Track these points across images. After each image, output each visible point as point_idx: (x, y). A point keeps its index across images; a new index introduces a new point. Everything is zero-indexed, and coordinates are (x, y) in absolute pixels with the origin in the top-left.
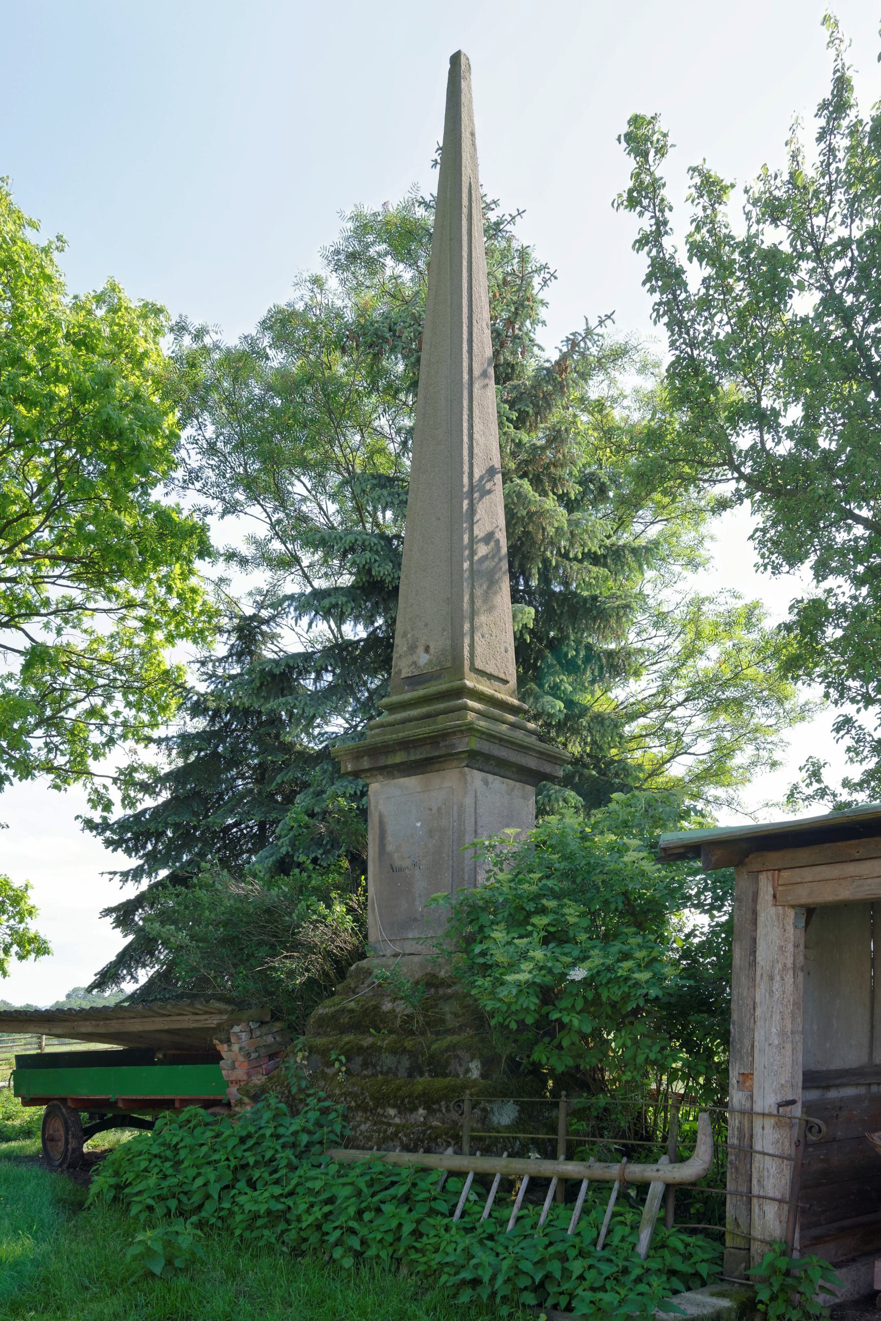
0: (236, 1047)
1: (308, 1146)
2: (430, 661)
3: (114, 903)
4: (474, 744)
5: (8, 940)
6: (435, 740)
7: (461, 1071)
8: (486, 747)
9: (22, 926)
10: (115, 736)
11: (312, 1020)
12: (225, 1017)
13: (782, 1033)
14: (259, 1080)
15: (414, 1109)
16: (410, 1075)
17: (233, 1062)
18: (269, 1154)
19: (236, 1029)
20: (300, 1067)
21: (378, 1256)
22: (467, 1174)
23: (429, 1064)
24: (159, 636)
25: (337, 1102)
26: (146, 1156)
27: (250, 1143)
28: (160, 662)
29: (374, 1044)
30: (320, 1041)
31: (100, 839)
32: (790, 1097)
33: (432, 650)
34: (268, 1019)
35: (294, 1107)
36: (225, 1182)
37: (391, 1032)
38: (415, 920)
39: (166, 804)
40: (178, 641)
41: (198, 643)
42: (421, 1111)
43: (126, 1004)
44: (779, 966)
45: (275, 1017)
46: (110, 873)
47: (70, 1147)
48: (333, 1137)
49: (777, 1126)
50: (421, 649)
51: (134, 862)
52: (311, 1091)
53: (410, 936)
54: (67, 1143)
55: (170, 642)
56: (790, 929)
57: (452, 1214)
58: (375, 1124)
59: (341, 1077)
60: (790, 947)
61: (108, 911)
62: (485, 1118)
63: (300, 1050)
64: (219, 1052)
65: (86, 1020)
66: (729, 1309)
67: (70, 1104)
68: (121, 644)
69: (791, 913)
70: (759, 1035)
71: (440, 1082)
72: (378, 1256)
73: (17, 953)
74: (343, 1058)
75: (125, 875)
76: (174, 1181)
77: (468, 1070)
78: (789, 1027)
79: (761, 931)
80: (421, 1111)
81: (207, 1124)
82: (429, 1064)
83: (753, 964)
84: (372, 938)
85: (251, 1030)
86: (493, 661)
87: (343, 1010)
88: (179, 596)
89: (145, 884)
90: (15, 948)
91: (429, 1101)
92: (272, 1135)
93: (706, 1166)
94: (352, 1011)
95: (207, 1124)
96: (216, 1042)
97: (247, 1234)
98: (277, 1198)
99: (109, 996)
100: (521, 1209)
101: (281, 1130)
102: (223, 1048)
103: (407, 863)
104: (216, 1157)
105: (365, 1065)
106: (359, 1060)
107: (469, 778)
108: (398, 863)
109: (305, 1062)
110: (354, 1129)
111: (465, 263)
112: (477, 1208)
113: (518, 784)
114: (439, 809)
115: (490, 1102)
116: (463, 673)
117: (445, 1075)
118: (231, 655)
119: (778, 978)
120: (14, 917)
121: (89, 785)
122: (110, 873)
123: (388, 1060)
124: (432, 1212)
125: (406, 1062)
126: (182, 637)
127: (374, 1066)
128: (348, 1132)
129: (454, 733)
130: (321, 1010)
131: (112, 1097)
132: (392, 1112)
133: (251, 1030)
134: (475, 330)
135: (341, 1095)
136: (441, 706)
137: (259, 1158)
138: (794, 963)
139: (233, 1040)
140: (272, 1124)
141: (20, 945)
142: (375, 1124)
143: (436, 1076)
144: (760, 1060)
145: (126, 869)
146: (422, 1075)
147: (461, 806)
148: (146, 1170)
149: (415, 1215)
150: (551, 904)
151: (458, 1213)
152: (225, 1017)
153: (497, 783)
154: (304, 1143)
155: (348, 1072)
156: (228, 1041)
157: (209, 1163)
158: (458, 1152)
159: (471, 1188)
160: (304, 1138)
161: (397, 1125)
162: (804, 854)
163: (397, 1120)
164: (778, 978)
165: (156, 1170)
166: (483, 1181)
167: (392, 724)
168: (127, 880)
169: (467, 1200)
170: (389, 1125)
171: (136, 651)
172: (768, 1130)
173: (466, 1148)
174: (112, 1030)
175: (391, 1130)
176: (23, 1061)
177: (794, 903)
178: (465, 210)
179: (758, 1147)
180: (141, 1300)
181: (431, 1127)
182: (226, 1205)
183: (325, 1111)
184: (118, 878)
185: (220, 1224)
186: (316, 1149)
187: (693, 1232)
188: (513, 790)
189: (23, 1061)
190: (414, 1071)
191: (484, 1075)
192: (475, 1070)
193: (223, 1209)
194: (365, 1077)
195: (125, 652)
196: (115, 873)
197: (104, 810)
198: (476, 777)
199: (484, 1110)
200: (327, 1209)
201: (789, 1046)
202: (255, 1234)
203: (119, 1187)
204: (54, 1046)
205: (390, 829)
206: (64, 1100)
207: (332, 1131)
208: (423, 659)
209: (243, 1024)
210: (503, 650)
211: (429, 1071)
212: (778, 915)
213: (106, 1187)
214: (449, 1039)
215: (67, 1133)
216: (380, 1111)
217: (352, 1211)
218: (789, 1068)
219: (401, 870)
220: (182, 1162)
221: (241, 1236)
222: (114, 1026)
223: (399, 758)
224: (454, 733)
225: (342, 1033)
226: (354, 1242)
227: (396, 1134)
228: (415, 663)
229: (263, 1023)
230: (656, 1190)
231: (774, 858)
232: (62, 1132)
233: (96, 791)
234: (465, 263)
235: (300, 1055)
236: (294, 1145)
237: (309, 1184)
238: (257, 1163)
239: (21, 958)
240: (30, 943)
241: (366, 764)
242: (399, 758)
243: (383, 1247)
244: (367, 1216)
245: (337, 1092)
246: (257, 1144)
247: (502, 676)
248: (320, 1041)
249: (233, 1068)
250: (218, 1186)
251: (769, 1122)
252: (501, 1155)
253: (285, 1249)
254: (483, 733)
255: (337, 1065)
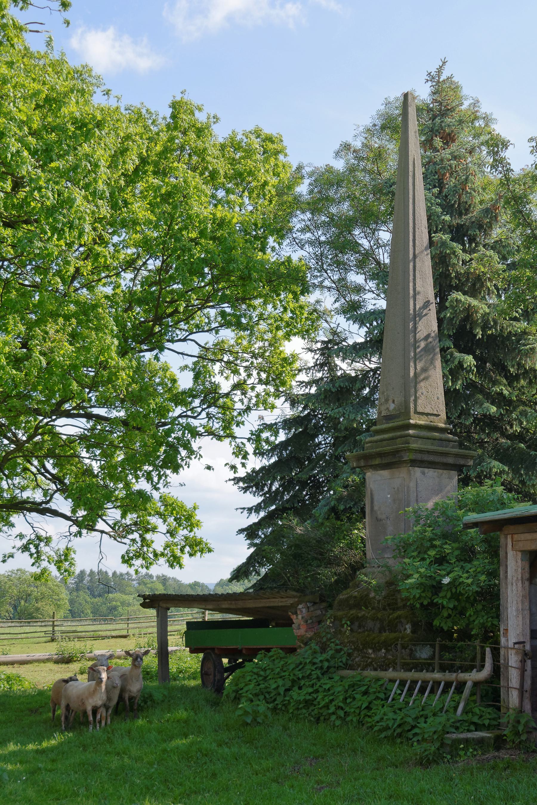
0: (300, 617)
1: (329, 668)
2: (395, 408)
3: (245, 526)
4: (412, 456)
5: (183, 543)
6: (395, 453)
7: (402, 629)
8: (419, 456)
9: (192, 534)
10: (251, 405)
11: (336, 602)
12: (296, 600)
13: (517, 610)
14: (309, 634)
15: (381, 650)
16: (380, 632)
17: (299, 625)
18: (308, 673)
19: (300, 606)
20: (329, 627)
21: (352, 720)
22: (396, 681)
23: (388, 626)
24: (280, 333)
25: (345, 646)
26: (251, 674)
27: (301, 667)
28: (281, 352)
29: (364, 615)
30: (340, 613)
31: (236, 487)
32: (522, 640)
33: (396, 403)
34: (318, 601)
35: (323, 650)
36: (287, 687)
37: (373, 609)
38: (388, 547)
39: (275, 463)
40: (292, 338)
41: (305, 339)
42: (383, 651)
43: (251, 591)
44: (515, 579)
45: (322, 600)
46: (241, 509)
47: (216, 678)
48: (341, 664)
49: (517, 653)
50: (390, 402)
51: (259, 499)
52: (332, 640)
53: (386, 556)
54: (215, 676)
55: (287, 339)
56: (519, 561)
57: (387, 699)
58: (363, 658)
59: (348, 633)
60: (520, 570)
61: (241, 531)
62: (411, 653)
63: (329, 618)
64: (292, 620)
65: (225, 600)
66: (489, 738)
67: (216, 651)
68: (256, 338)
69: (520, 554)
70: (509, 610)
71: (393, 635)
72: (352, 720)
73: (188, 552)
74: (349, 623)
75: (250, 510)
76: (262, 686)
77: (405, 629)
78: (520, 607)
79: (509, 563)
80: (383, 651)
81: (281, 658)
82: (388, 626)
83: (506, 577)
84: (368, 557)
85: (308, 607)
86: (429, 406)
87: (351, 597)
88: (292, 312)
89: (262, 514)
90: (187, 549)
91: (387, 645)
92: (310, 662)
93: (489, 673)
94: (355, 597)
95: (281, 658)
96: (290, 613)
97: (296, 712)
98: (310, 694)
99: (238, 588)
100: (417, 695)
101: (315, 660)
102: (294, 617)
103: (384, 517)
104: (283, 674)
105: (360, 627)
106: (357, 624)
107: (412, 472)
108: (380, 517)
109: (331, 625)
110: (352, 660)
111: (411, 201)
112: (399, 697)
113: (445, 471)
114: (398, 489)
115: (414, 645)
116: (410, 416)
117: (395, 632)
118: (316, 365)
119: (514, 584)
120: (186, 528)
121: (233, 443)
122: (241, 509)
123: (370, 624)
124: (377, 698)
125: (378, 625)
126: (295, 335)
127: (364, 627)
128: (350, 662)
129: (402, 451)
130: (342, 596)
131: (239, 647)
132: (370, 651)
133: (308, 607)
134: (417, 233)
135: (348, 642)
136: (399, 434)
137: (304, 674)
138: (522, 577)
139: (298, 612)
140: (311, 657)
141: (191, 546)
142: (363, 658)
143: (392, 632)
144: (510, 623)
145: (250, 506)
146: (385, 632)
147: (408, 487)
148: (250, 681)
149: (369, 699)
150: (437, 543)
151: (390, 699)
152: (296, 600)
153: (431, 473)
154: (325, 667)
155: (352, 630)
156: (296, 613)
157: (281, 677)
158: (395, 669)
159: (398, 687)
160: (326, 664)
161: (372, 658)
162: (521, 528)
163: (373, 656)
164: (514, 584)
165: (255, 681)
166: (403, 683)
167: (376, 442)
168: (251, 513)
169: (395, 693)
170: (369, 658)
171: (267, 344)
172: (513, 656)
173: (398, 668)
174: (239, 607)
175: (370, 660)
176: (190, 625)
177: (523, 549)
178: (411, 174)
179: (510, 664)
180: (241, 735)
181: (388, 659)
182: (287, 698)
183: (338, 651)
184: (246, 512)
185: (283, 708)
186: (332, 670)
187: (489, 706)
188: (442, 475)
189: (190, 625)
190: (382, 630)
191: (413, 632)
192: (408, 628)
193: (285, 700)
194: (360, 633)
195: (260, 344)
196: (244, 509)
197: (243, 458)
198: (417, 471)
199: (411, 650)
200: (331, 698)
201: (520, 616)
202: (299, 712)
203: (236, 691)
204: (209, 616)
205: (376, 498)
206: (213, 649)
207: (341, 662)
208: (392, 406)
209: (304, 604)
210: (436, 398)
211: (389, 629)
212: (513, 555)
213: (231, 691)
214: (399, 613)
215: (215, 670)
216: (365, 651)
217: (341, 698)
218: (521, 626)
219: (381, 520)
220: (267, 676)
221: (292, 713)
222: (240, 604)
223: (377, 461)
224: (402, 451)
225: (350, 609)
226: (341, 713)
227: (371, 663)
228: (388, 408)
229: (315, 603)
230: (469, 684)
231: (512, 528)
232: (212, 670)
233: (238, 447)
234: (411, 201)
235: (329, 620)
236: (321, 668)
237: (324, 687)
238: (303, 677)
239: (191, 555)
240: (196, 546)
241: (362, 463)
242: (377, 461)
243: (355, 716)
244: (349, 701)
245: (346, 641)
246: (303, 667)
247: (435, 412)
248: (340, 613)
249: (299, 629)
250: (283, 689)
251: (513, 652)
252: (411, 671)
253: (312, 719)
254: (416, 450)
255: (345, 626)
